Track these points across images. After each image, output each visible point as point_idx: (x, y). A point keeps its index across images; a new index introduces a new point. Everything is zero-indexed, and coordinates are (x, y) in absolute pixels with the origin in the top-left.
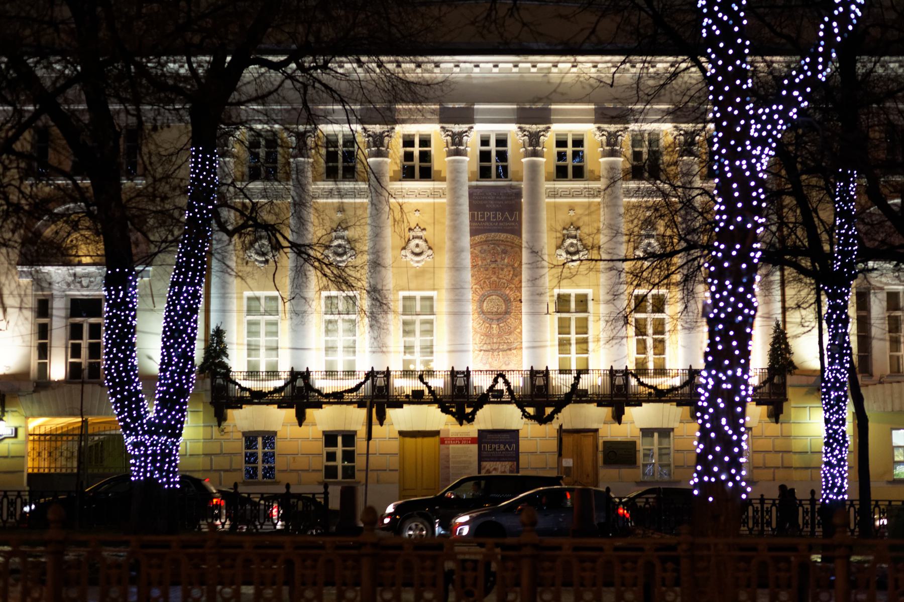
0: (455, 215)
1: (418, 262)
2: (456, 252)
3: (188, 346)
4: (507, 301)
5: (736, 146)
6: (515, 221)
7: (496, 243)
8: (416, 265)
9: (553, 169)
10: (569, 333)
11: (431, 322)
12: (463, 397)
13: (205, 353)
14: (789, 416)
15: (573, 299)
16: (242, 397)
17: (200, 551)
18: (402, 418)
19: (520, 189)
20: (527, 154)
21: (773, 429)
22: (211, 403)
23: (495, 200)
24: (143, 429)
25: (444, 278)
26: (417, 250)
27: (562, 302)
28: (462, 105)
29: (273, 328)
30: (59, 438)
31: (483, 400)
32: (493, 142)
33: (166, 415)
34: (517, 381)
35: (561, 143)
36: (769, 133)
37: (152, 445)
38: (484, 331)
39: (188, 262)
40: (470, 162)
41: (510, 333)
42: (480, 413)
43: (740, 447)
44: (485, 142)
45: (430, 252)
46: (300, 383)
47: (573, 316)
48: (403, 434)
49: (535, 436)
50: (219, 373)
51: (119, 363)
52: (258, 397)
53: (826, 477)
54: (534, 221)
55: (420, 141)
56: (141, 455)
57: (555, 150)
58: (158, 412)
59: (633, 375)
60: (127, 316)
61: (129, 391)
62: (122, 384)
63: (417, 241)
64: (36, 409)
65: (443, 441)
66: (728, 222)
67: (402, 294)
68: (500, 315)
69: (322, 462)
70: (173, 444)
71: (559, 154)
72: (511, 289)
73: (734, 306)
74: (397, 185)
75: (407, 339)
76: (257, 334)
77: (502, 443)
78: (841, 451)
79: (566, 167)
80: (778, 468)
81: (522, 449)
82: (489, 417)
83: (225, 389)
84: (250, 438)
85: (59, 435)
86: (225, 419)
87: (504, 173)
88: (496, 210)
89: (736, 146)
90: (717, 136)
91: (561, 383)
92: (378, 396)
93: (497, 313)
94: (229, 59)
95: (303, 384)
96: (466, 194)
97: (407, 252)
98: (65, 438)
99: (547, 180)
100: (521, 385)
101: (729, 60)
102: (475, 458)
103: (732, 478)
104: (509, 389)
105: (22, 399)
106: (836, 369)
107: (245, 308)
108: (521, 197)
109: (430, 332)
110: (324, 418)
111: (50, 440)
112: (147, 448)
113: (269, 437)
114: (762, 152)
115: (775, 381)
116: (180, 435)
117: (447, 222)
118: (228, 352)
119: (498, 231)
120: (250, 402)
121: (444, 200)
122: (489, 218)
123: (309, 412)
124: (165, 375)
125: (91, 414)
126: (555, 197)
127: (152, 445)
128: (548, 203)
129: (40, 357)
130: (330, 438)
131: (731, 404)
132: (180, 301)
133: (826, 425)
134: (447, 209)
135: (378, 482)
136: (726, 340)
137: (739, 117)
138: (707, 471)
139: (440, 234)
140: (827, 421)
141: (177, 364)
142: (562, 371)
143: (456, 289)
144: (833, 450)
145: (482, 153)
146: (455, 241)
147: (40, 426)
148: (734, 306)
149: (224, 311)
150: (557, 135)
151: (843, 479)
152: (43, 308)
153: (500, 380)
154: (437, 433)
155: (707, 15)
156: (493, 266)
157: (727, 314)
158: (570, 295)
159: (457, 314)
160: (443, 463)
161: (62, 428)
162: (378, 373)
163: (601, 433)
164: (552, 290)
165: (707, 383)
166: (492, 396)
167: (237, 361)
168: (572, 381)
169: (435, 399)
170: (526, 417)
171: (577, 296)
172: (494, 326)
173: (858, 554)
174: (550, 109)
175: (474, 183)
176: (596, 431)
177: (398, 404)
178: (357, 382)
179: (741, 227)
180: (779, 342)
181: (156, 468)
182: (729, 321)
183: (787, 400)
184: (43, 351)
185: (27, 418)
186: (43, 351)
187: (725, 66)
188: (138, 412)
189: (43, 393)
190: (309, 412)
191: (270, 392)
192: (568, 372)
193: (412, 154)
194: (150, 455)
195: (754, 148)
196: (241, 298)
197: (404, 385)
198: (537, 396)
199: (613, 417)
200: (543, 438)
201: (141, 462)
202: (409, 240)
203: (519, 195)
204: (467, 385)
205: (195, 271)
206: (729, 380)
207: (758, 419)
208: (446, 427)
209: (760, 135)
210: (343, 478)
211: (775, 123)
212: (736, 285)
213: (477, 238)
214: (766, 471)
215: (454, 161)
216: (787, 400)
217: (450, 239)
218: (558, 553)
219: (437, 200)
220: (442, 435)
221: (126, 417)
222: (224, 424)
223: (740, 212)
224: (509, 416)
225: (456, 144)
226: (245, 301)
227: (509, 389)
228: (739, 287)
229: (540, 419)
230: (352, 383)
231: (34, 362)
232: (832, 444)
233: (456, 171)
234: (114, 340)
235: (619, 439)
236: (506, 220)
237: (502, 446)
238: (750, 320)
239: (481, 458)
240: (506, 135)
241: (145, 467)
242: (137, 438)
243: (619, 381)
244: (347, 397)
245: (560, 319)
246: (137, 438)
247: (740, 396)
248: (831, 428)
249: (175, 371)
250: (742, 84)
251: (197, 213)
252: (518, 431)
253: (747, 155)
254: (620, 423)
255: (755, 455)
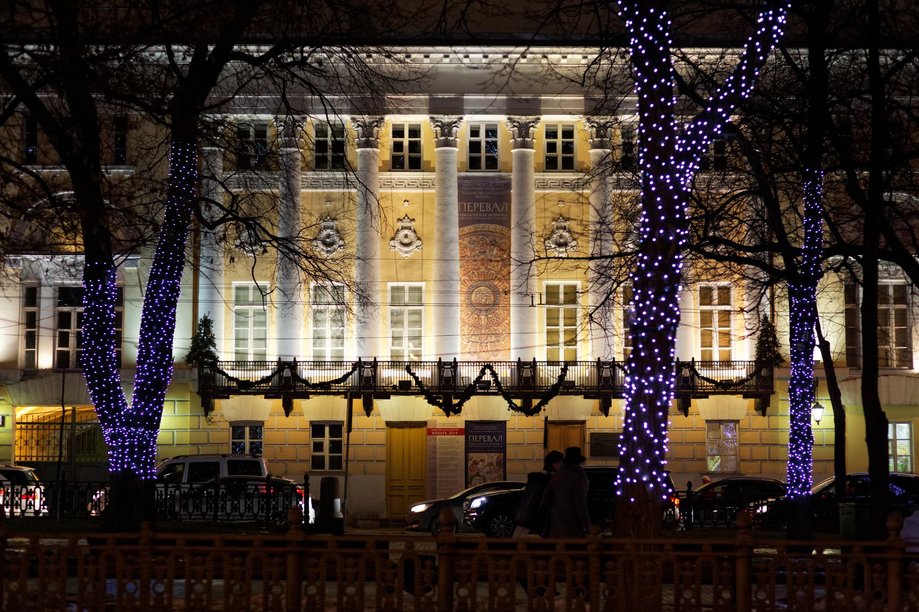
0: (444, 205)
1: (407, 252)
2: (445, 243)
3: (166, 338)
4: (495, 292)
5: (660, 161)
6: (504, 212)
7: (485, 234)
8: (405, 255)
9: (542, 160)
10: (558, 325)
11: (419, 313)
12: (450, 388)
13: (193, 342)
14: (777, 408)
15: (562, 290)
16: (229, 387)
17: (134, 547)
18: (390, 408)
19: (510, 180)
20: (516, 146)
21: (761, 421)
22: (198, 393)
23: (485, 191)
24: (120, 420)
25: (433, 269)
26: (406, 241)
27: (552, 294)
28: (452, 96)
29: (262, 318)
30: (46, 427)
31: (470, 391)
32: (482, 133)
33: (143, 408)
34: (504, 373)
35: (551, 134)
36: (694, 148)
37: (130, 436)
38: (472, 322)
39: (167, 256)
40: (459, 153)
41: (499, 324)
42: (467, 405)
43: (661, 450)
44: (475, 132)
45: (419, 243)
46: (287, 373)
47: (562, 308)
48: (389, 424)
49: (522, 428)
50: (206, 363)
51: (97, 356)
52: (245, 387)
53: (790, 473)
54: (524, 212)
55: (410, 131)
56: (119, 447)
57: (545, 141)
58: (135, 404)
59: (620, 367)
60: (105, 309)
61: (107, 383)
62: (100, 376)
63: (406, 232)
64: (23, 398)
65: (430, 432)
66: (651, 235)
67: (391, 284)
68: (488, 309)
69: (308, 453)
70: (151, 435)
71: (549, 144)
72: (499, 280)
73: (657, 315)
74: (387, 175)
75: (395, 329)
76: (245, 324)
77: (489, 434)
78: (805, 447)
79: (555, 158)
80: (765, 460)
81: (509, 440)
82: (476, 408)
83: (213, 378)
84: (237, 428)
85: (46, 423)
86: (212, 409)
87: (492, 163)
88: (486, 201)
89: (660, 161)
90: (642, 151)
91: (549, 375)
92: (365, 385)
93: (486, 305)
94: (211, 48)
95: (290, 375)
96: (456, 185)
97: (395, 243)
98: (52, 427)
99: (537, 171)
100: (509, 375)
101: (654, 79)
102: (462, 450)
103: (653, 479)
104: (496, 380)
105: (9, 387)
106: (802, 367)
107: (233, 299)
108: (510, 188)
109: (419, 323)
110: (312, 408)
111: (38, 429)
112: (124, 439)
113: (257, 428)
114: (686, 166)
115: (762, 374)
116: (158, 426)
117: (436, 213)
118: (216, 342)
119: (487, 222)
120: (237, 392)
121: (433, 191)
122: (478, 209)
123: (297, 402)
124: (143, 368)
125: (79, 403)
126: (544, 188)
127: (130, 436)
128: (537, 194)
129: (28, 346)
130: (317, 428)
131: (653, 409)
132: (158, 294)
133: (792, 422)
134: (436, 199)
135: (365, 472)
136: (649, 347)
137: (664, 133)
138: (630, 473)
139: (429, 225)
140: (793, 418)
141: (155, 357)
142: (550, 363)
143: (445, 280)
144: (798, 446)
145: (471, 143)
146: (444, 232)
147: (27, 415)
148: (657, 315)
149: (212, 302)
150: (547, 126)
151: (808, 475)
152: (31, 297)
153: (488, 371)
154: (423, 424)
155: (634, 35)
156: (482, 257)
157: (649, 322)
158: (558, 287)
159: (445, 305)
160: (431, 453)
161: (50, 416)
162: (365, 363)
163: (588, 425)
164: (539, 286)
165: (631, 388)
166: (479, 387)
167: (225, 351)
168: (559, 373)
169: (422, 389)
170: (513, 409)
171: (565, 287)
172: (483, 317)
173: (831, 548)
174: (540, 100)
175: (463, 174)
176: (583, 422)
177: (385, 394)
178: (345, 372)
179: (663, 239)
180: (766, 336)
181: (133, 460)
182: (652, 329)
183: (774, 393)
184: (31, 340)
185: (14, 406)
186: (31, 340)
187: (650, 84)
188: (116, 404)
189: (30, 382)
190: (297, 402)
191: (257, 382)
192: (556, 363)
193: (401, 144)
194: (127, 447)
195: (678, 162)
196: (230, 288)
197: (391, 375)
198: (524, 387)
199: (601, 409)
200: (530, 429)
201: (119, 453)
202: (398, 230)
203: (508, 186)
204: (455, 376)
205: (173, 264)
206: (651, 385)
207: (745, 412)
208: (434, 418)
209: (685, 150)
210: (330, 468)
211: (699, 139)
212: (658, 295)
213: (466, 229)
214: (754, 463)
215: (444, 152)
216: (774, 393)
217: (439, 230)
218: (475, 551)
219: (426, 191)
220: (429, 426)
221: (104, 409)
222: (211, 414)
223: (663, 225)
224: (494, 408)
225: (446, 136)
226: (233, 292)
227: (496, 380)
228: (661, 296)
229: (528, 410)
230: (339, 374)
231: (22, 350)
232: (797, 440)
233: (445, 162)
234: (92, 333)
235: (606, 431)
236: (495, 211)
237: (489, 438)
238: (672, 328)
239: (468, 450)
240: (496, 125)
241: (123, 459)
242: (114, 430)
243: (606, 373)
244: (335, 388)
245: (548, 310)
246: (114, 430)
247: (661, 401)
248: (796, 425)
249: (153, 364)
250: (666, 102)
251: (177, 207)
252: (505, 422)
253: (671, 170)
254: (607, 415)
255: (743, 448)
